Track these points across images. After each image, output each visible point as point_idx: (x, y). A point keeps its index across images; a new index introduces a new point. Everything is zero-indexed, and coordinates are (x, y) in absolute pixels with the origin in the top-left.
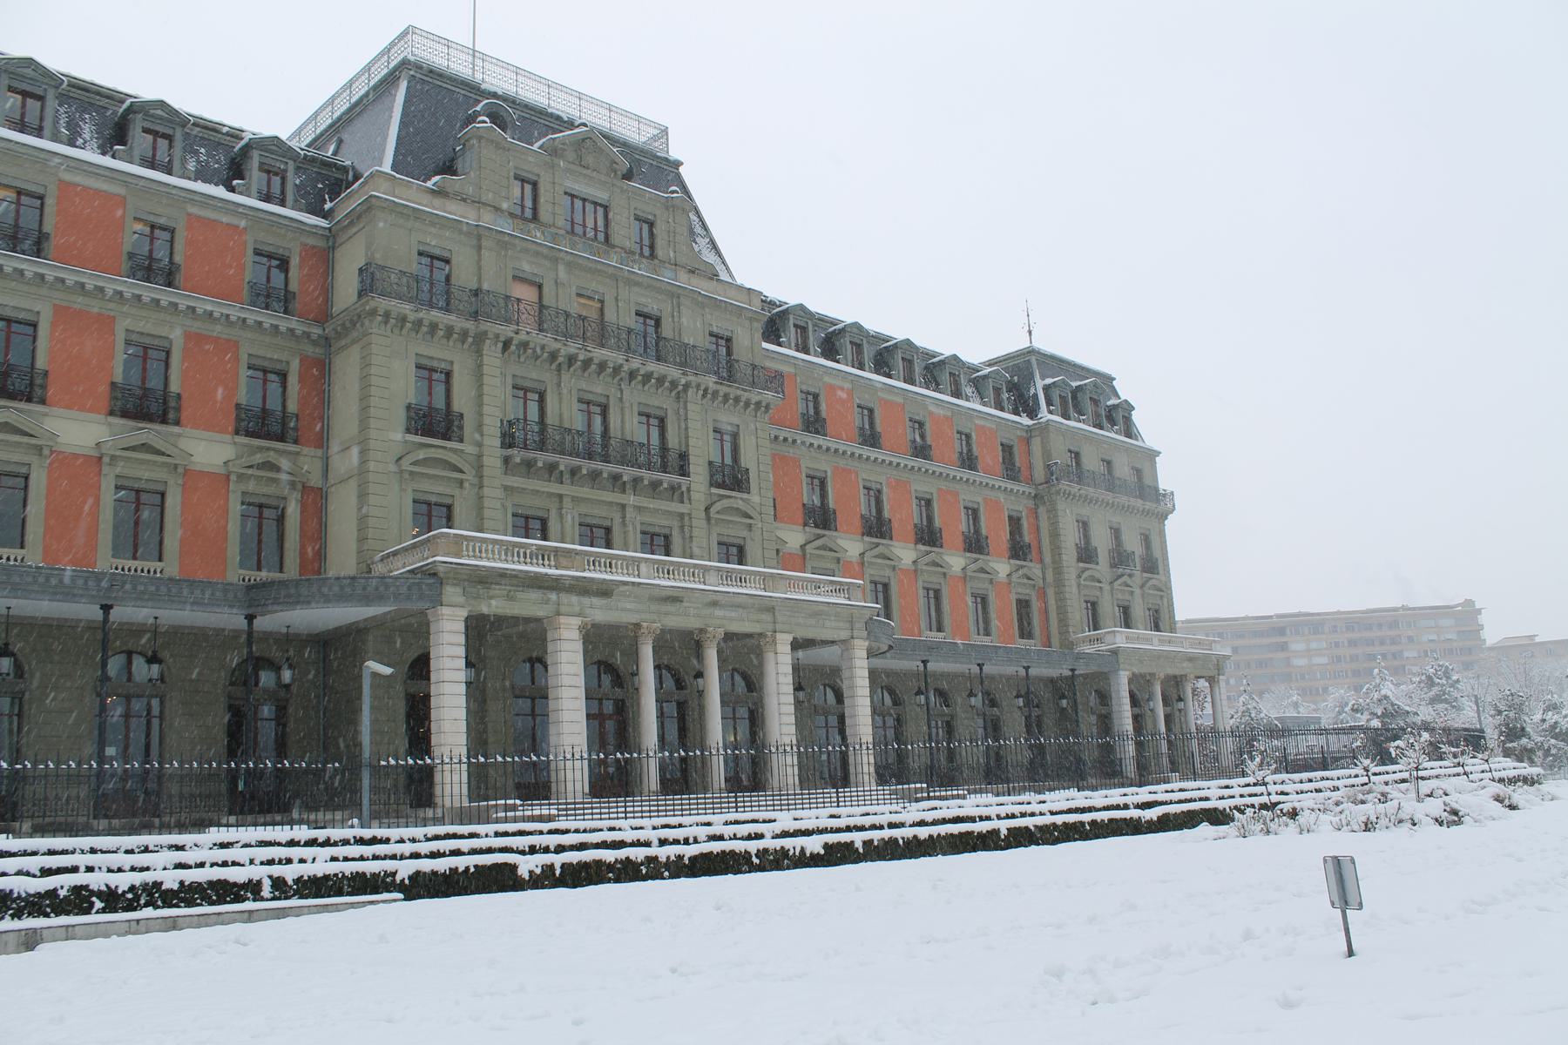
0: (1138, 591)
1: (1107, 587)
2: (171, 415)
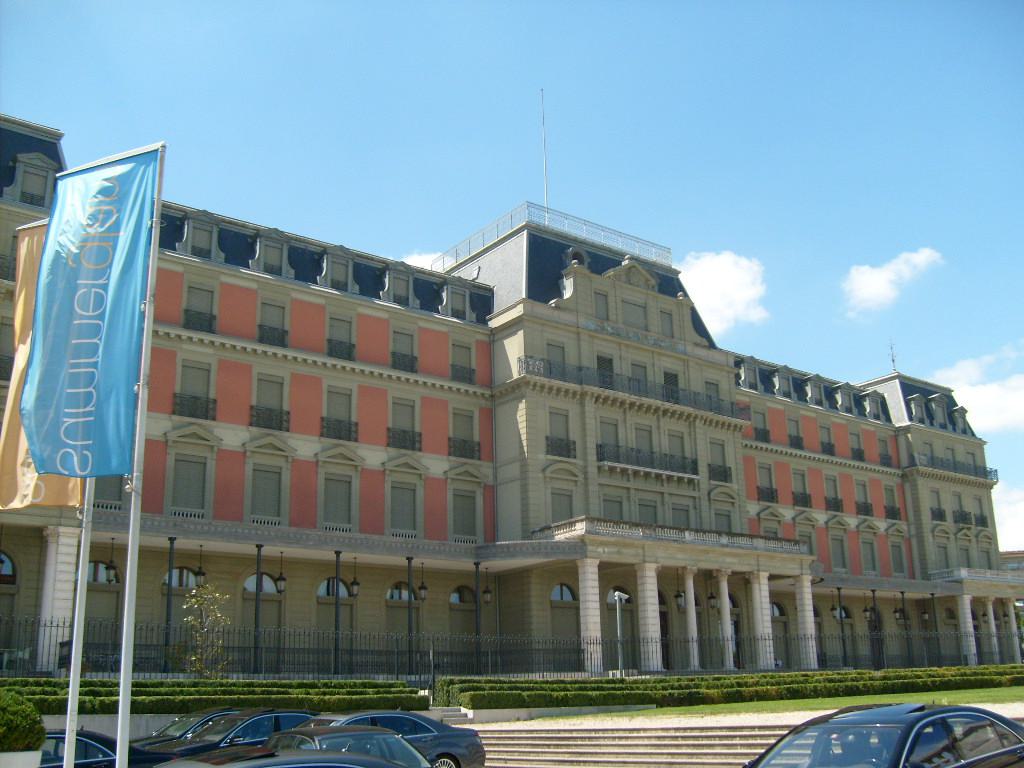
0: (974, 540)
1: (952, 537)
2: (417, 445)
